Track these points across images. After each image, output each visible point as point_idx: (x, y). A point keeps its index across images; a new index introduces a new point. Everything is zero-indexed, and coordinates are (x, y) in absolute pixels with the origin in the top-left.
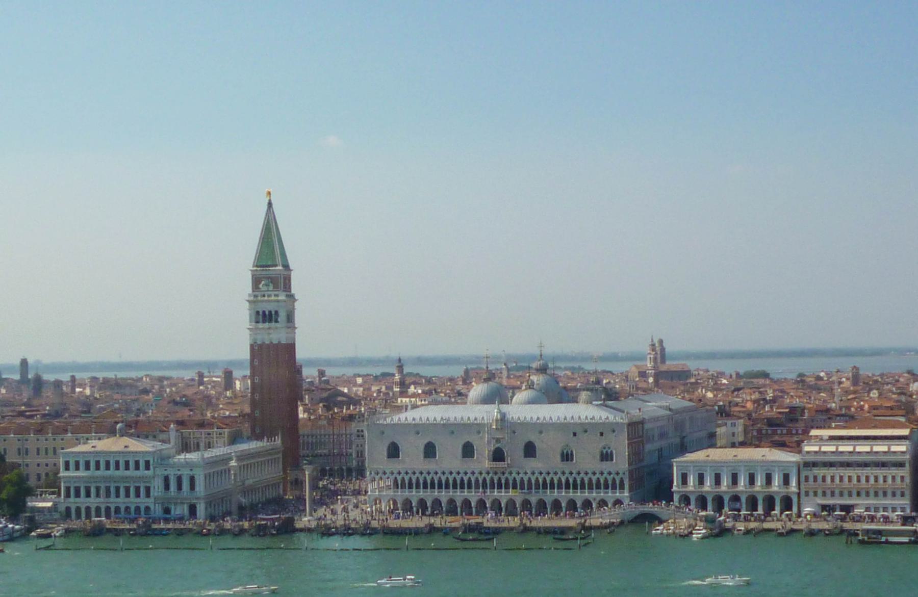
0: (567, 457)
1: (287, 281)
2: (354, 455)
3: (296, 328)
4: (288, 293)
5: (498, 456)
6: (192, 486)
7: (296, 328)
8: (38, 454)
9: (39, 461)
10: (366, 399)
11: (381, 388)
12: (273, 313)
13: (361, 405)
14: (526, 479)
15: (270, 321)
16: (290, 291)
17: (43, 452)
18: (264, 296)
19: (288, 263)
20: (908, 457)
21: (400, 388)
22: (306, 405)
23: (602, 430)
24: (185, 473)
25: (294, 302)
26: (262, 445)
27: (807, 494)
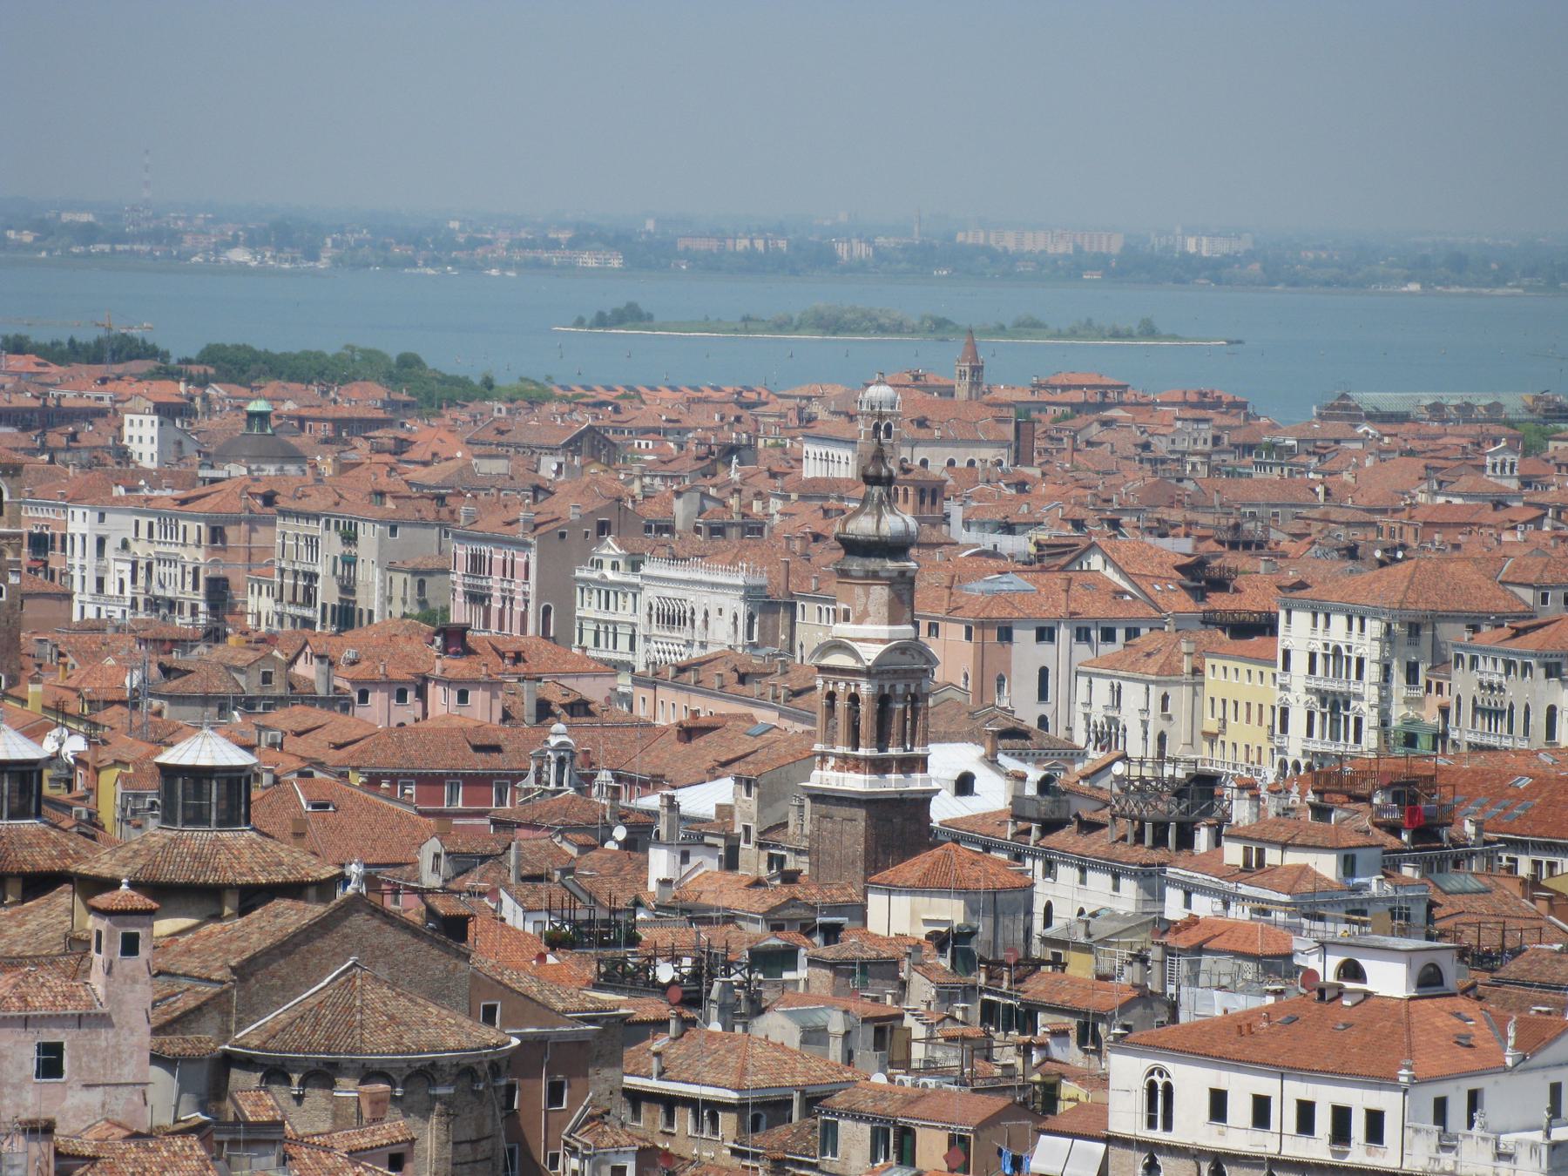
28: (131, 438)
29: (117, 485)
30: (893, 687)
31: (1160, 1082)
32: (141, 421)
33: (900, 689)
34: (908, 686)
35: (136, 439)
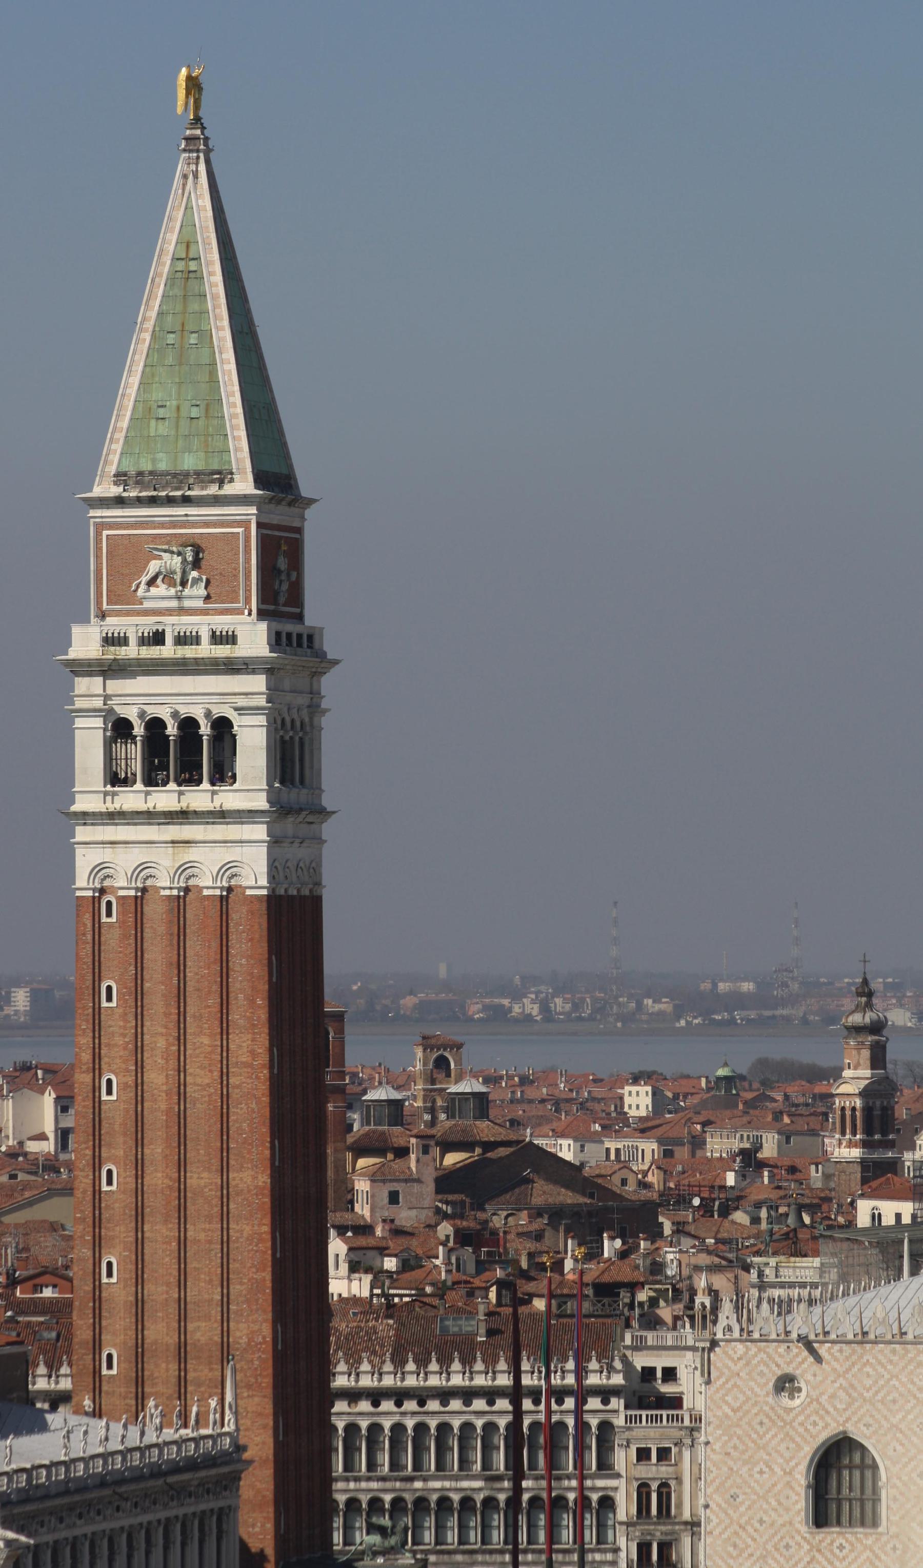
1: (282, 563)
2: (625, 1507)
3: (323, 813)
4: (290, 627)
7: (323, 813)
10: (683, 1201)
11: (758, 1147)
12: (205, 729)
13: (655, 1233)
16: (300, 617)
18: (158, 638)
19: (290, 467)
21: (865, 1144)
22: (364, 1229)
25: (317, 674)
26: (133, 1438)
28: (630, 1106)
29: (595, 1123)
30: (874, 1103)
31: (876, 1212)
32: (638, 1093)
33: (878, 1103)
34: (882, 1102)
35: (634, 1107)
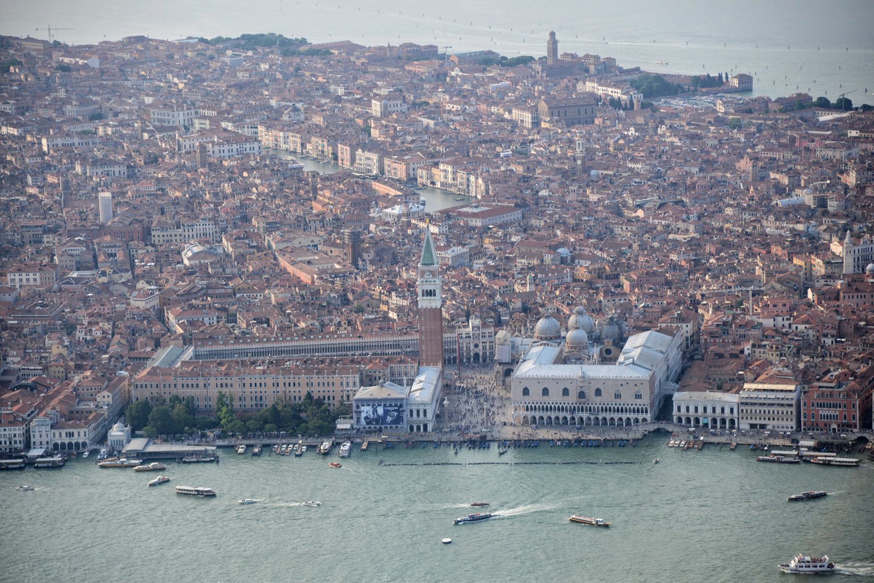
0: (618, 396)
5: (582, 395)
6: (425, 415)
8: (319, 385)
9: (329, 389)
14: (596, 407)
15: (431, 295)
17: (321, 384)
20: (125, 437)
23: (636, 383)
24: (422, 408)
27: (743, 418)
